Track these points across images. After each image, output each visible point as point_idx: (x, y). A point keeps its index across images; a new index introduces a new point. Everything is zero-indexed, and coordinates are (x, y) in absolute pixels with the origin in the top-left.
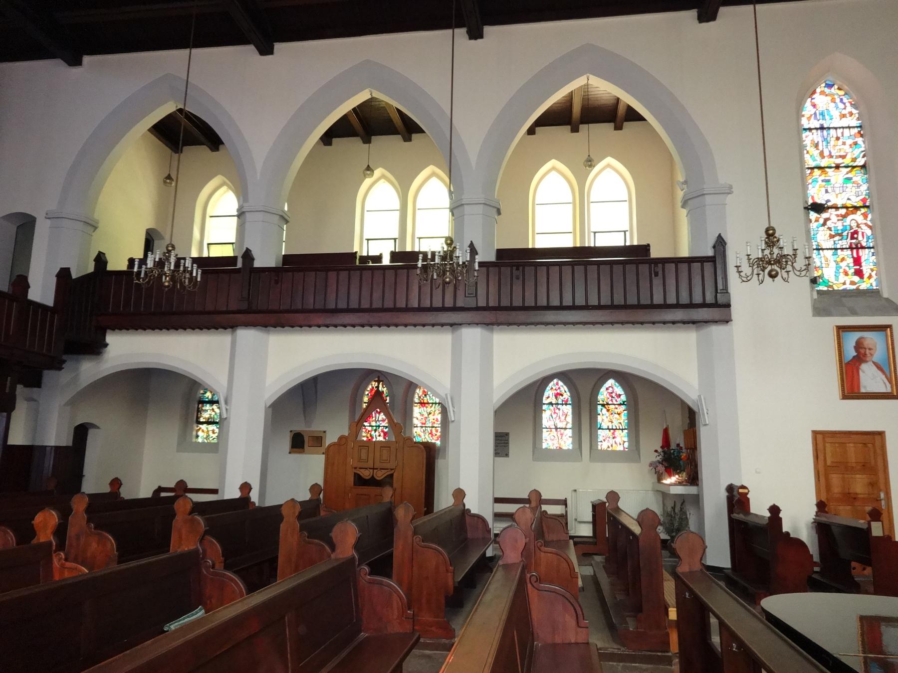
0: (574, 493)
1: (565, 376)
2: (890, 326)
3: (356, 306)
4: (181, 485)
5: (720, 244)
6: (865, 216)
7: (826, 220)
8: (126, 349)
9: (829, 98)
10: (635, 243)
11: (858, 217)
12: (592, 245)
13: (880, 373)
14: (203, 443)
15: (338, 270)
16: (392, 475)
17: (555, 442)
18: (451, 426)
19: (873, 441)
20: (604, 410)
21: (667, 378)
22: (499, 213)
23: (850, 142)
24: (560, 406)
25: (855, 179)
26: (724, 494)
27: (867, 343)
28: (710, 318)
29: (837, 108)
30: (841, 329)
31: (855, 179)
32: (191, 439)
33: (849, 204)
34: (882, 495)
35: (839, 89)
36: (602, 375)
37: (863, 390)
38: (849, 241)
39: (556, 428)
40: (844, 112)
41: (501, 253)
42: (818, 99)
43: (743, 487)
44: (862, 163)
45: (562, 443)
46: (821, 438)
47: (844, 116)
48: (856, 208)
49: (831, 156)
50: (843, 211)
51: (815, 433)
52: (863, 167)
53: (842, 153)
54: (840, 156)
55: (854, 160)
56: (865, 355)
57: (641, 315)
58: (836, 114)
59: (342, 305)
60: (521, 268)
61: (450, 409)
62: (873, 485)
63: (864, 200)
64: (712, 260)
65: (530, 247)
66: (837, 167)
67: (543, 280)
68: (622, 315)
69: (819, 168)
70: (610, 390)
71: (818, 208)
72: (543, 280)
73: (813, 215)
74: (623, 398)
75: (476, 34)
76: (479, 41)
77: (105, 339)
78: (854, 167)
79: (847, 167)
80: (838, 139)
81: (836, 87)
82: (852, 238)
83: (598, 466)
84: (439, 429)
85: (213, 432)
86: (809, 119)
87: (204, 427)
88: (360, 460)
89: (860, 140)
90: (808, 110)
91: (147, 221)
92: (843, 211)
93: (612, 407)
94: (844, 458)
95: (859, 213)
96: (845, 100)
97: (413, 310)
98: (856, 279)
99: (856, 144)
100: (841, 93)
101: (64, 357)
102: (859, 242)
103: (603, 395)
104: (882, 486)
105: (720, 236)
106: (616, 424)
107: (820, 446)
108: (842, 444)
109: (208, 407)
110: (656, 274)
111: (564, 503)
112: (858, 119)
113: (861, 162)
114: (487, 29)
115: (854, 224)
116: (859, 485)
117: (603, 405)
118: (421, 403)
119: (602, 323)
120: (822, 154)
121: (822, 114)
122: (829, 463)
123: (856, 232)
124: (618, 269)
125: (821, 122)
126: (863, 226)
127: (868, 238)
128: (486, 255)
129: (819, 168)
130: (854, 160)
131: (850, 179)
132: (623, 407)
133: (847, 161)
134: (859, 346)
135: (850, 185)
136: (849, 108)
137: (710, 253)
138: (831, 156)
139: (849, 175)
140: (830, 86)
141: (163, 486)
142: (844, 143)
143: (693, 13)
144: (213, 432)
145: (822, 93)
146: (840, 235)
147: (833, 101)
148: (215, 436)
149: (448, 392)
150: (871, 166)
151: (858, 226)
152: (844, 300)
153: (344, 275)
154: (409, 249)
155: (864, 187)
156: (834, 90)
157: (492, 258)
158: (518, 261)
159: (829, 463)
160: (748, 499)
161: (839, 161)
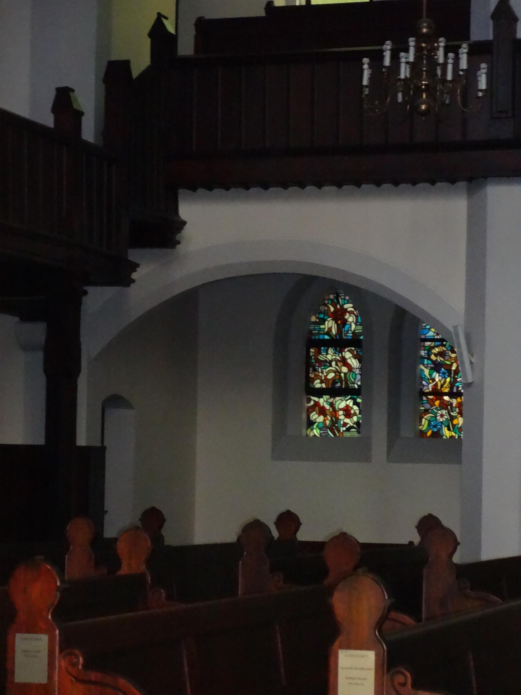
8: (225, 231)
109: (331, 355)
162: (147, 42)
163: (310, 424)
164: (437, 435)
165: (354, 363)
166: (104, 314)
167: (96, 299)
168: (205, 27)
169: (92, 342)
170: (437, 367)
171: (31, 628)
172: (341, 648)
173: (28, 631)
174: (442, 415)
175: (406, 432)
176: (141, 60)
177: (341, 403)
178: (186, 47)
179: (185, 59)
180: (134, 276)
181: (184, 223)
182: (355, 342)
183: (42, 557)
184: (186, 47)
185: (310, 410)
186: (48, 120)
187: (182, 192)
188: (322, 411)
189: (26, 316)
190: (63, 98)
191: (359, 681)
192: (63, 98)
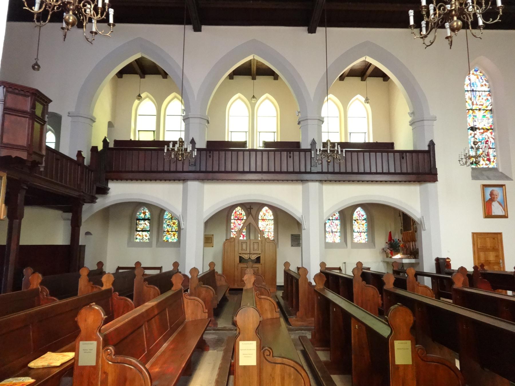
0: (344, 264)
1: (243, 205)
2: (504, 185)
3: (254, 170)
4: (138, 264)
5: (432, 144)
6: (491, 133)
7: (475, 134)
8: (119, 191)
9: (476, 77)
10: (279, 141)
11: (488, 133)
12: (137, 139)
13: (500, 207)
14: (140, 242)
15: (219, 151)
16: (260, 257)
17: (332, 239)
18: (182, 231)
19: (497, 237)
20: (356, 223)
21: (406, 207)
22: (208, 123)
23: (485, 98)
24: (334, 221)
25: (487, 116)
26: (434, 262)
27: (495, 193)
28: (332, 179)
29: (479, 81)
30: (485, 186)
31: (487, 116)
32: (134, 239)
33: (484, 127)
34: (501, 261)
35: (480, 72)
36: (261, 205)
37: (493, 214)
38: (485, 145)
39: (332, 232)
40: (482, 84)
41: (210, 143)
42: (473, 78)
43: (448, 258)
44: (490, 109)
45: (335, 239)
46: (476, 236)
47: (482, 86)
48: (488, 130)
49: (477, 105)
50: (482, 131)
51: (473, 234)
52: (491, 110)
53: (482, 103)
54: (481, 105)
55: (487, 107)
56: (494, 198)
57: (211, 175)
58: (479, 84)
59: (247, 169)
60: (292, 153)
61: (182, 222)
62: (497, 256)
63: (491, 126)
64: (428, 152)
65: (226, 140)
66: (480, 110)
67: (234, 158)
68: (330, 177)
69: (472, 109)
70: (359, 213)
71: (473, 129)
72: (234, 158)
73: (470, 132)
74: (365, 217)
75: (197, 29)
76: (313, 34)
77: (108, 185)
78: (487, 110)
79: (484, 110)
80: (480, 96)
81: (479, 71)
82: (486, 143)
83: (355, 250)
84: (273, 233)
85: (146, 236)
86: (467, 86)
87: (140, 233)
88: (242, 249)
89: (489, 98)
90: (467, 82)
91: (109, 119)
92: (482, 131)
93: (359, 221)
94: (488, 244)
95: (489, 132)
96: (483, 78)
97: (247, 172)
98: (488, 162)
99: (487, 99)
100: (481, 74)
101: (97, 196)
102: (489, 146)
103: (355, 216)
104: (501, 257)
105: (314, 139)
106: (361, 230)
107: (475, 239)
108: (485, 238)
109: (142, 222)
110: (290, 157)
111: (340, 269)
112: (488, 88)
113: (489, 108)
114: (203, 27)
115: (487, 137)
116: (492, 257)
117: (355, 220)
118: (262, 220)
119: (269, 180)
120: (473, 104)
121: (473, 84)
122: (479, 247)
123: (487, 141)
124: (355, 155)
125: (472, 88)
126: (490, 138)
127: (493, 144)
128: (201, 144)
129: (472, 109)
130: (487, 107)
131: (485, 116)
132: (365, 221)
133: (484, 107)
134: (492, 194)
135: (485, 119)
136: (485, 82)
137: (426, 148)
138: (477, 105)
139: (485, 114)
140: (476, 71)
141: (120, 266)
142: (482, 99)
143: (306, 28)
144: (146, 236)
145: (473, 74)
146: (481, 142)
147: (478, 78)
148: (147, 238)
149: (181, 214)
150: (494, 110)
151: (488, 138)
152: (484, 172)
153: (222, 154)
154: (161, 139)
155: (491, 120)
156: (478, 73)
157: (204, 146)
158: (217, 147)
159: (479, 247)
160: (450, 264)
161: (480, 107)
162: (102, 143)
163: (137, 239)
164: (167, 241)
165: (148, 224)
166: (88, 211)
167: (86, 207)
168: (116, 142)
169: (85, 216)
170: (168, 225)
171: (88, 338)
172: (241, 340)
173: (87, 340)
174: (169, 236)
175: (160, 240)
176: (100, 148)
177: (144, 233)
178: (111, 145)
179: (111, 149)
180: (97, 201)
181: (109, 189)
182: (148, 219)
183: (94, 303)
184: (111, 145)
185: (136, 235)
186: (75, 158)
187: (109, 181)
188: (140, 236)
189: (65, 211)
190: (79, 153)
191: (248, 355)
192: (79, 153)
